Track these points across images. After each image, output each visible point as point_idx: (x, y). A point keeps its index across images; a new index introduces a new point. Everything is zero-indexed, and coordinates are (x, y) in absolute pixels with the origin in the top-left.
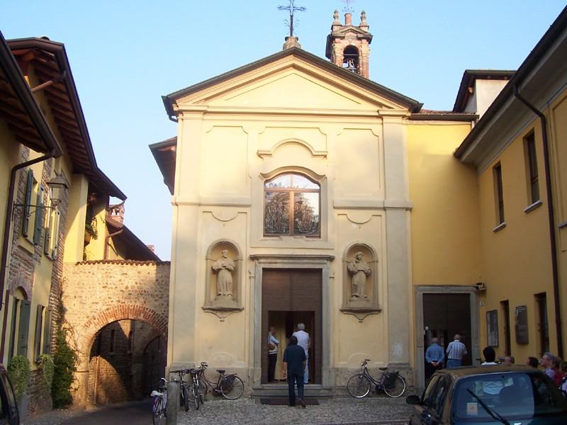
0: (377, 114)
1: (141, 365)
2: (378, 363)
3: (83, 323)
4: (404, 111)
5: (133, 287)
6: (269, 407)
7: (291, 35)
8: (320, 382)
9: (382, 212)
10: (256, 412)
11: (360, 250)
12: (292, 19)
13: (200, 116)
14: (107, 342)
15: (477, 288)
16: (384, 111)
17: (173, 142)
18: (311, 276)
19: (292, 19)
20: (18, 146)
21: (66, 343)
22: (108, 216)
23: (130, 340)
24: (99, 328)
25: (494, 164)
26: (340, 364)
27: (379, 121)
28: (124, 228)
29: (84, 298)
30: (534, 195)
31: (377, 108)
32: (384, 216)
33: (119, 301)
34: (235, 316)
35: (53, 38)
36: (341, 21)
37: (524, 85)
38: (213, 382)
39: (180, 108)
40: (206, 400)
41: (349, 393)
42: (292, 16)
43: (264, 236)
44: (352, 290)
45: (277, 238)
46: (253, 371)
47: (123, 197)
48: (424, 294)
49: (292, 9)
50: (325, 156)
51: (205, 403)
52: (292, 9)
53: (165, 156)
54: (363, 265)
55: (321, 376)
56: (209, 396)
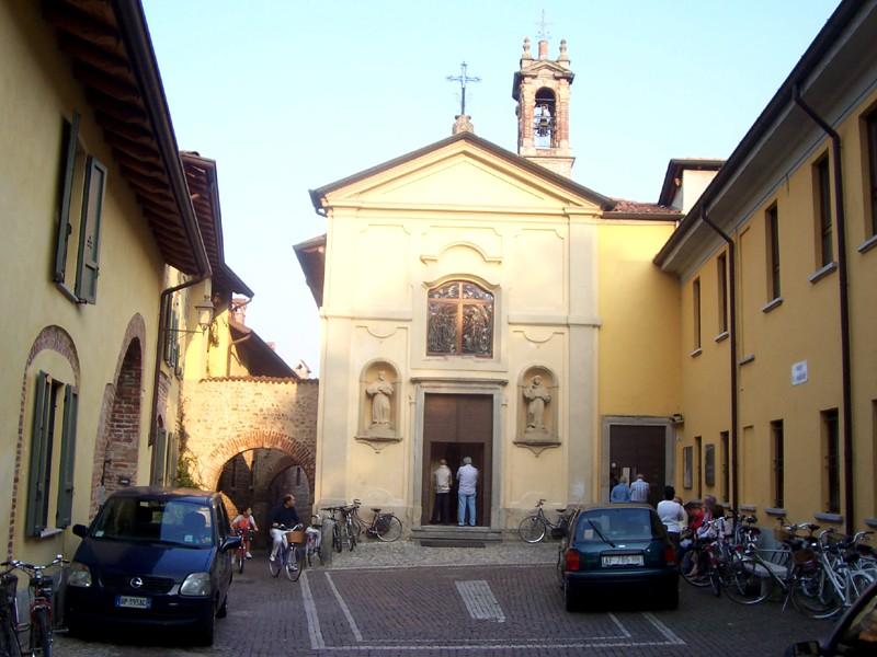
0: (562, 212)
1: (264, 504)
2: (556, 503)
3: (209, 453)
4: (596, 209)
5: (268, 409)
6: (430, 549)
7: (463, 113)
8: (489, 524)
9: (565, 330)
10: (416, 553)
11: (539, 373)
12: (463, 93)
13: (354, 212)
14: (233, 476)
15: (674, 420)
16: (570, 209)
17: (322, 242)
18: (479, 403)
19: (463, 93)
20: (164, 267)
21: (188, 475)
22: (232, 318)
23: (252, 472)
24: (228, 458)
25: (694, 279)
26: (513, 504)
27: (566, 220)
28: (252, 333)
29: (209, 421)
30: (825, 257)
31: (561, 205)
32: (567, 334)
33: (252, 426)
34: (391, 447)
35: (203, 155)
36: (533, 53)
37: (713, 205)
38: (367, 522)
39: (331, 204)
40: (360, 542)
41: (521, 536)
42: (464, 89)
43: (428, 355)
44: (528, 419)
45: (441, 358)
46: (413, 511)
47: (250, 294)
48: (612, 426)
49: (464, 79)
50: (500, 262)
51: (358, 544)
52: (464, 79)
53: (312, 260)
54: (541, 391)
55: (489, 518)
56: (363, 537)
